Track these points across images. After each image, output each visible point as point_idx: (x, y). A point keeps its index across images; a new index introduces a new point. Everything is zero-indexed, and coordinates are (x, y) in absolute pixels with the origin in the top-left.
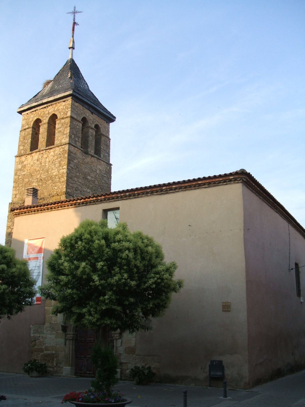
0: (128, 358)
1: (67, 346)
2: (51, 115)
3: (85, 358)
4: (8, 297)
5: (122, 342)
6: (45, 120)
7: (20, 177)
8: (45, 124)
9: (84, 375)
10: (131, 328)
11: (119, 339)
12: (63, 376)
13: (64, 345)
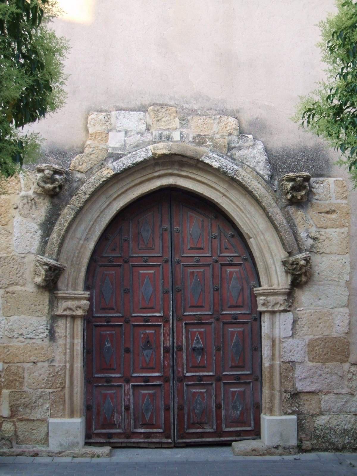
0: (321, 375)
1: (61, 341)
3: (127, 381)
5: (295, 322)
9: (126, 440)
10: (38, 151)
11: (285, 311)
12: (50, 455)
13: (46, 340)
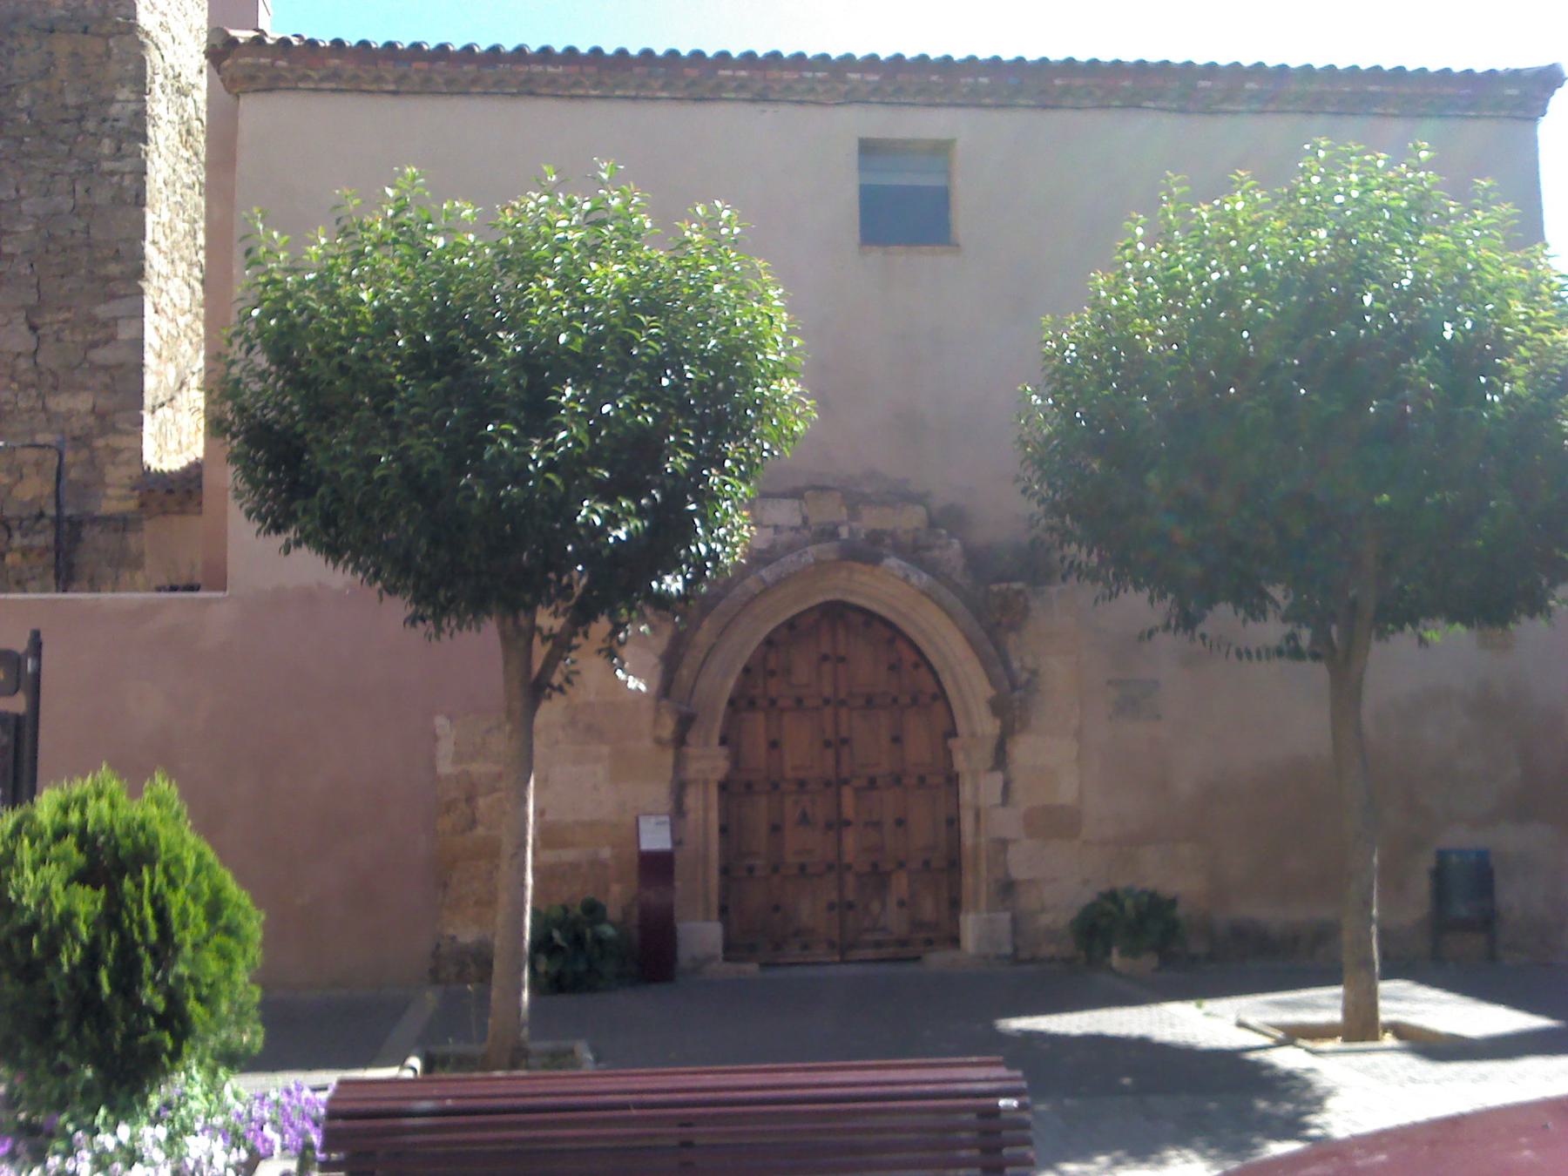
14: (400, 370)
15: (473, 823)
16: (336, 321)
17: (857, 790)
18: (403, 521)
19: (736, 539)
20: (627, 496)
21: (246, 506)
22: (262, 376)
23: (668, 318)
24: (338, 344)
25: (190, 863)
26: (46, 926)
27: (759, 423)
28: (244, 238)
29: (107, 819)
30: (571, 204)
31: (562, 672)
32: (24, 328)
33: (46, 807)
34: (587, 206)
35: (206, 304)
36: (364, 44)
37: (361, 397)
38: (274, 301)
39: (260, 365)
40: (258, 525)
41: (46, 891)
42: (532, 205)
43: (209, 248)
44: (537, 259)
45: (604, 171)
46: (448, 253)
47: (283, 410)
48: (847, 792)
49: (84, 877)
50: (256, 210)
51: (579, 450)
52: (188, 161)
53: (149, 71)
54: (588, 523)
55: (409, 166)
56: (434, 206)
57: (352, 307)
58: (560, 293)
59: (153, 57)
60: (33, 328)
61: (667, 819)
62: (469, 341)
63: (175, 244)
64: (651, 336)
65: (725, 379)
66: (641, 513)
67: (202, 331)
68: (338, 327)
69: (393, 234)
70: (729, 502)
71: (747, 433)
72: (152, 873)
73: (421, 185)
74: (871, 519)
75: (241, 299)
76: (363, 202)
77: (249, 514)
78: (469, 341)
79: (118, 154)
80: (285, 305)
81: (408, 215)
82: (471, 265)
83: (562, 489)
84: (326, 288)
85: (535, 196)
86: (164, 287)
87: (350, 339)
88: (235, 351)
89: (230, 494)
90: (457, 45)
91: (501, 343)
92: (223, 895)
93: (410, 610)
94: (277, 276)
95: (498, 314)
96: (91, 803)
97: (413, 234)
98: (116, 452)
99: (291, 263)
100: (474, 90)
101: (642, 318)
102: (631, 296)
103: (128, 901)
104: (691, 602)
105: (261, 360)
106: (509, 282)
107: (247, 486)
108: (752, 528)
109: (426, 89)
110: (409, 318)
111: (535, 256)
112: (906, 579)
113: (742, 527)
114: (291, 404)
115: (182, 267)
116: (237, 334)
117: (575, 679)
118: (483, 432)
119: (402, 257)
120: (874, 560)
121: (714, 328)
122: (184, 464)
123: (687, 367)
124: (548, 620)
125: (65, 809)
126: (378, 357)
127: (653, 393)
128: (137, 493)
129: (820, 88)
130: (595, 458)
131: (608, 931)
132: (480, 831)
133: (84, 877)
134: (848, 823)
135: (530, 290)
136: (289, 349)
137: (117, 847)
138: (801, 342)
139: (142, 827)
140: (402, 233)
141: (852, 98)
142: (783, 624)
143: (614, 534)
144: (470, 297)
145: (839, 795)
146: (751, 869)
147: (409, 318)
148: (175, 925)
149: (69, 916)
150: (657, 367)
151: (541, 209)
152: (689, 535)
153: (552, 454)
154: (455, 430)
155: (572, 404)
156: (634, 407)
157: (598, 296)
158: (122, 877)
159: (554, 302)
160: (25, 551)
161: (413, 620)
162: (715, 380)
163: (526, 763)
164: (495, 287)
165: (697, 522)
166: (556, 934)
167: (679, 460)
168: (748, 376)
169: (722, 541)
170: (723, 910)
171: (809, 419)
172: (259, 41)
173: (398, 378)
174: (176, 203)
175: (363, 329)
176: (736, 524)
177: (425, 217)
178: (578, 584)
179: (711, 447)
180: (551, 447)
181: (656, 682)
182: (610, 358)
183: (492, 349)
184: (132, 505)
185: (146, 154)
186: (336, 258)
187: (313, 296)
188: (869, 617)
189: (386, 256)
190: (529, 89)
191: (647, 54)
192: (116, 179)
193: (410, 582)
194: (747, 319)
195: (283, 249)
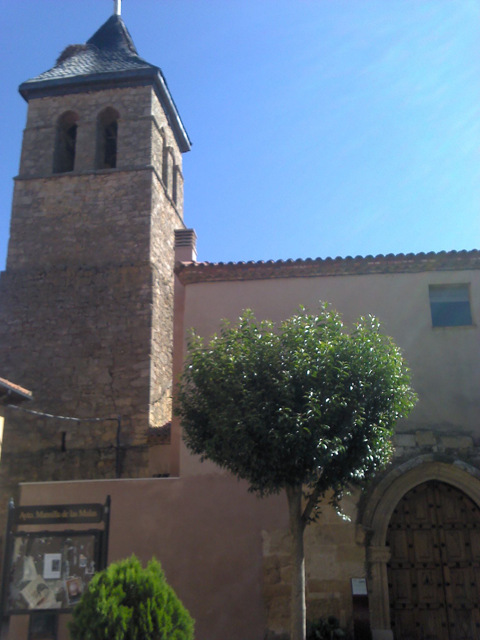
2: (102, 108)
4: (320, 376)
6: (92, 116)
7: (29, 222)
8: (89, 123)
14: (245, 388)
15: (279, 579)
16: (221, 369)
17: (450, 568)
18: (247, 448)
19: (386, 453)
20: (338, 436)
21: (188, 443)
22: (193, 391)
23: (351, 362)
24: (221, 378)
25: (166, 597)
26: (110, 623)
27: (393, 403)
28: (188, 339)
29: (134, 577)
30: (311, 319)
31: (314, 512)
32: (108, 375)
33: (111, 572)
34: (317, 319)
35: (173, 362)
36: (231, 263)
37: (230, 398)
38: (198, 362)
39: (193, 387)
40: (191, 450)
41: (111, 608)
42: (295, 320)
43: (175, 341)
44: (298, 341)
45: (324, 306)
46: (263, 340)
47: (200, 403)
48: (447, 570)
49: (124, 602)
50: (192, 328)
51: (317, 417)
52: (167, 309)
53: (154, 277)
54: (322, 448)
55: (248, 309)
56: (258, 323)
57: (227, 364)
58: (307, 354)
59: (155, 272)
60: (111, 374)
61: (364, 580)
62: (272, 375)
63: (162, 341)
64: (345, 370)
65: (377, 386)
66: (344, 443)
67: (171, 372)
68: (221, 371)
69: (242, 335)
70: (382, 438)
71: (388, 408)
72: (151, 600)
73: (252, 315)
74: (447, 443)
75: (186, 362)
76: (231, 323)
77: (188, 445)
78: (272, 375)
79: (143, 308)
80: (202, 364)
81: (248, 327)
82: (272, 345)
83: (310, 433)
84: (217, 357)
85: (296, 317)
86: (158, 356)
87: (226, 376)
88: (184, 382)
89: (181, 438)
90: (265, 261)
91: (284, 375)
92: (179, 611)
93: (250, 485)
94: (199, 353)
95: (283, 363)
96: (128, 570)
97: (249, 334)
98: (140, 420)
99: (205, 347)
100: (272, 277)
101: (341, 362)
102: (336, 354)
103: (142, 613)
104: (369, 481)
105: (193, 385)
106: (286, 350)
107: (188, 435)
108: (394, 448)
109: (254, 278)
110: (249, 366)
111: (297, 340)
112: (465, 470)
113: (389, 447)
114: (204, 401)
115: (164, 349)
116: (184, 375)
117: (319, 515)
118: (278, 411)
119: (245, 343)
120: (450, 461)
121: (371, 365)
122: (164, 424)
123: (360, 382)
124: (307, 489)
125: (118, 572)
126: (236, 383)
127: (346, 393)
128: (146, 437)
129: (410, 266)
130: (324, 420)
131: (341, 632)
132: (282, 583)
133: (124, 602)
134: (448, 584)
135: (295, 353)
136: (203, 380)
137: (137, 590)
138: (409, 369)
139: (147, 581)
140: (245, 334)
141: (424, 269)
142: (410, 491)
143: (333, 452)
144: (271, 357)
145: (443, 570)
146: (404, 605)
147: (249, 366)
148: (160, 624)
149: (119, 619)
150: (348, 382)
151: (299, 322)
152: (366, 453)
153: (306, 419)
154: (266, 411)
155: (313, 399)
156: (339, 399)
157: (322, 354)
158: (139, 602)
159: (305, 358)
160: (105, 461)
161: (252, 489)
162: (373, 386)
163: (300, 553)
164: (281, 353)
165: (369, 447)
166: (318, 633)
167: (359, 420)
168: (387, 385)
169: (380, 454)
170: (393, 624)
171: (415, 401)
172: (192, 265)
173: (244, 390)
174: (163, 324)
175: (231, 372)
176: (386, 447)
177: (254, 327)
178: (319, 474)
179: (373, 414)
180: (305, 417)
181: (355, 517)
182: (329, 379)
183: (280, 377)
184: (145, 441)
185: (153, 308)
186: (221, 344)
187: (212, 360)
188: (451, 488)
189: (239, 343)
190: (293, 275)
191: (339, 259)
192: (141, 317)
193: (250, 474)
194: (385, 361)
195: (201, 343)
